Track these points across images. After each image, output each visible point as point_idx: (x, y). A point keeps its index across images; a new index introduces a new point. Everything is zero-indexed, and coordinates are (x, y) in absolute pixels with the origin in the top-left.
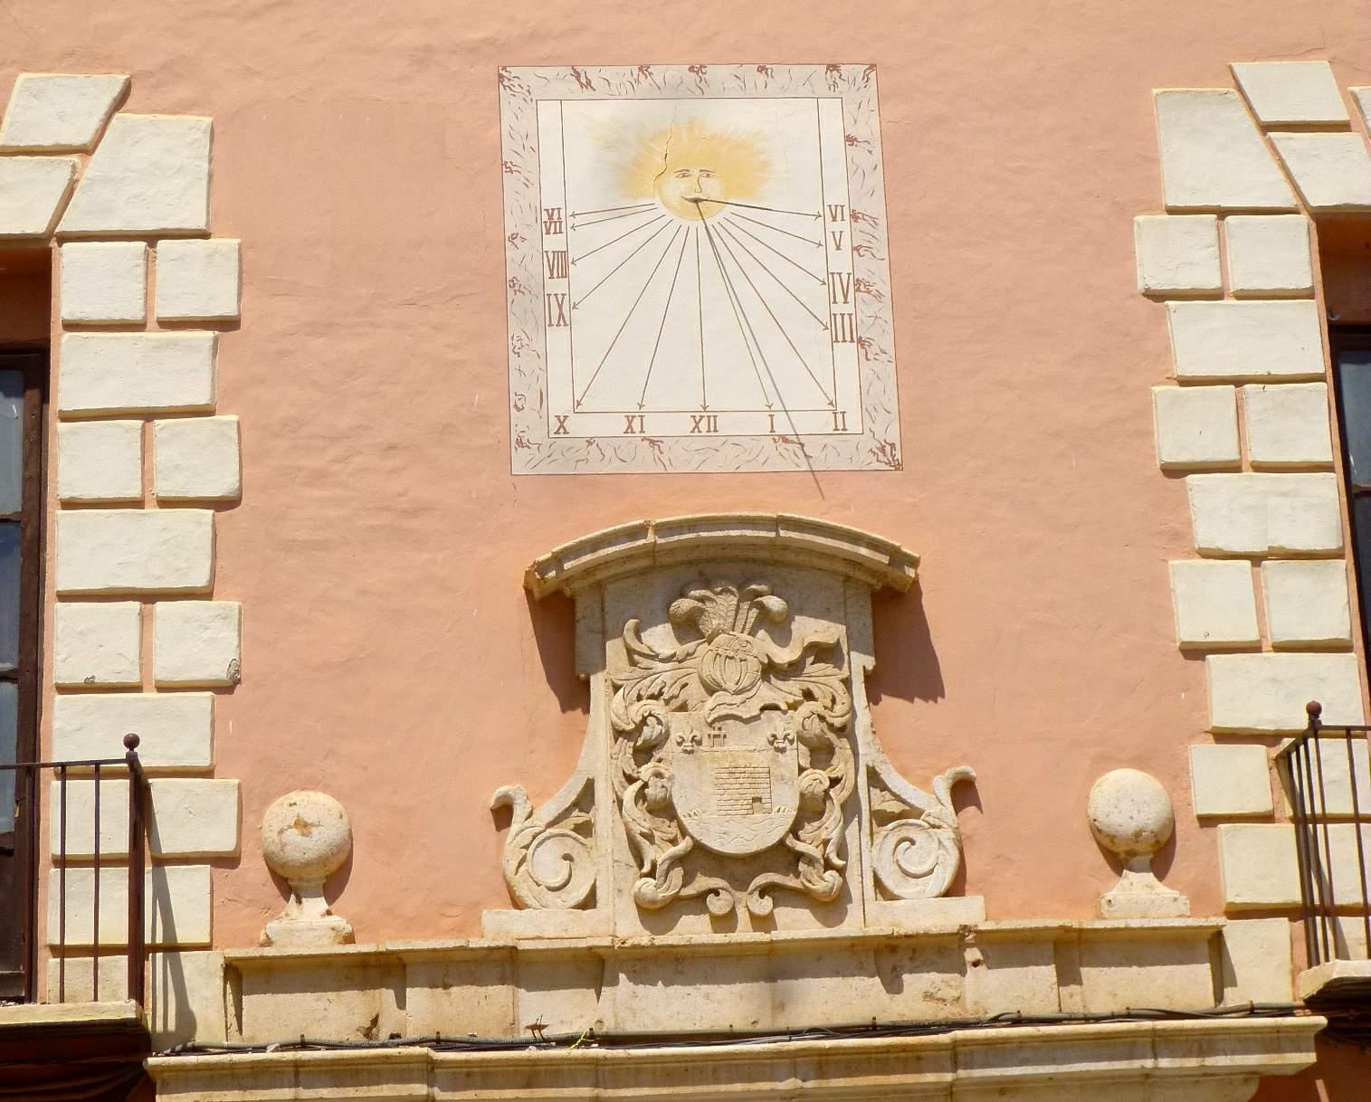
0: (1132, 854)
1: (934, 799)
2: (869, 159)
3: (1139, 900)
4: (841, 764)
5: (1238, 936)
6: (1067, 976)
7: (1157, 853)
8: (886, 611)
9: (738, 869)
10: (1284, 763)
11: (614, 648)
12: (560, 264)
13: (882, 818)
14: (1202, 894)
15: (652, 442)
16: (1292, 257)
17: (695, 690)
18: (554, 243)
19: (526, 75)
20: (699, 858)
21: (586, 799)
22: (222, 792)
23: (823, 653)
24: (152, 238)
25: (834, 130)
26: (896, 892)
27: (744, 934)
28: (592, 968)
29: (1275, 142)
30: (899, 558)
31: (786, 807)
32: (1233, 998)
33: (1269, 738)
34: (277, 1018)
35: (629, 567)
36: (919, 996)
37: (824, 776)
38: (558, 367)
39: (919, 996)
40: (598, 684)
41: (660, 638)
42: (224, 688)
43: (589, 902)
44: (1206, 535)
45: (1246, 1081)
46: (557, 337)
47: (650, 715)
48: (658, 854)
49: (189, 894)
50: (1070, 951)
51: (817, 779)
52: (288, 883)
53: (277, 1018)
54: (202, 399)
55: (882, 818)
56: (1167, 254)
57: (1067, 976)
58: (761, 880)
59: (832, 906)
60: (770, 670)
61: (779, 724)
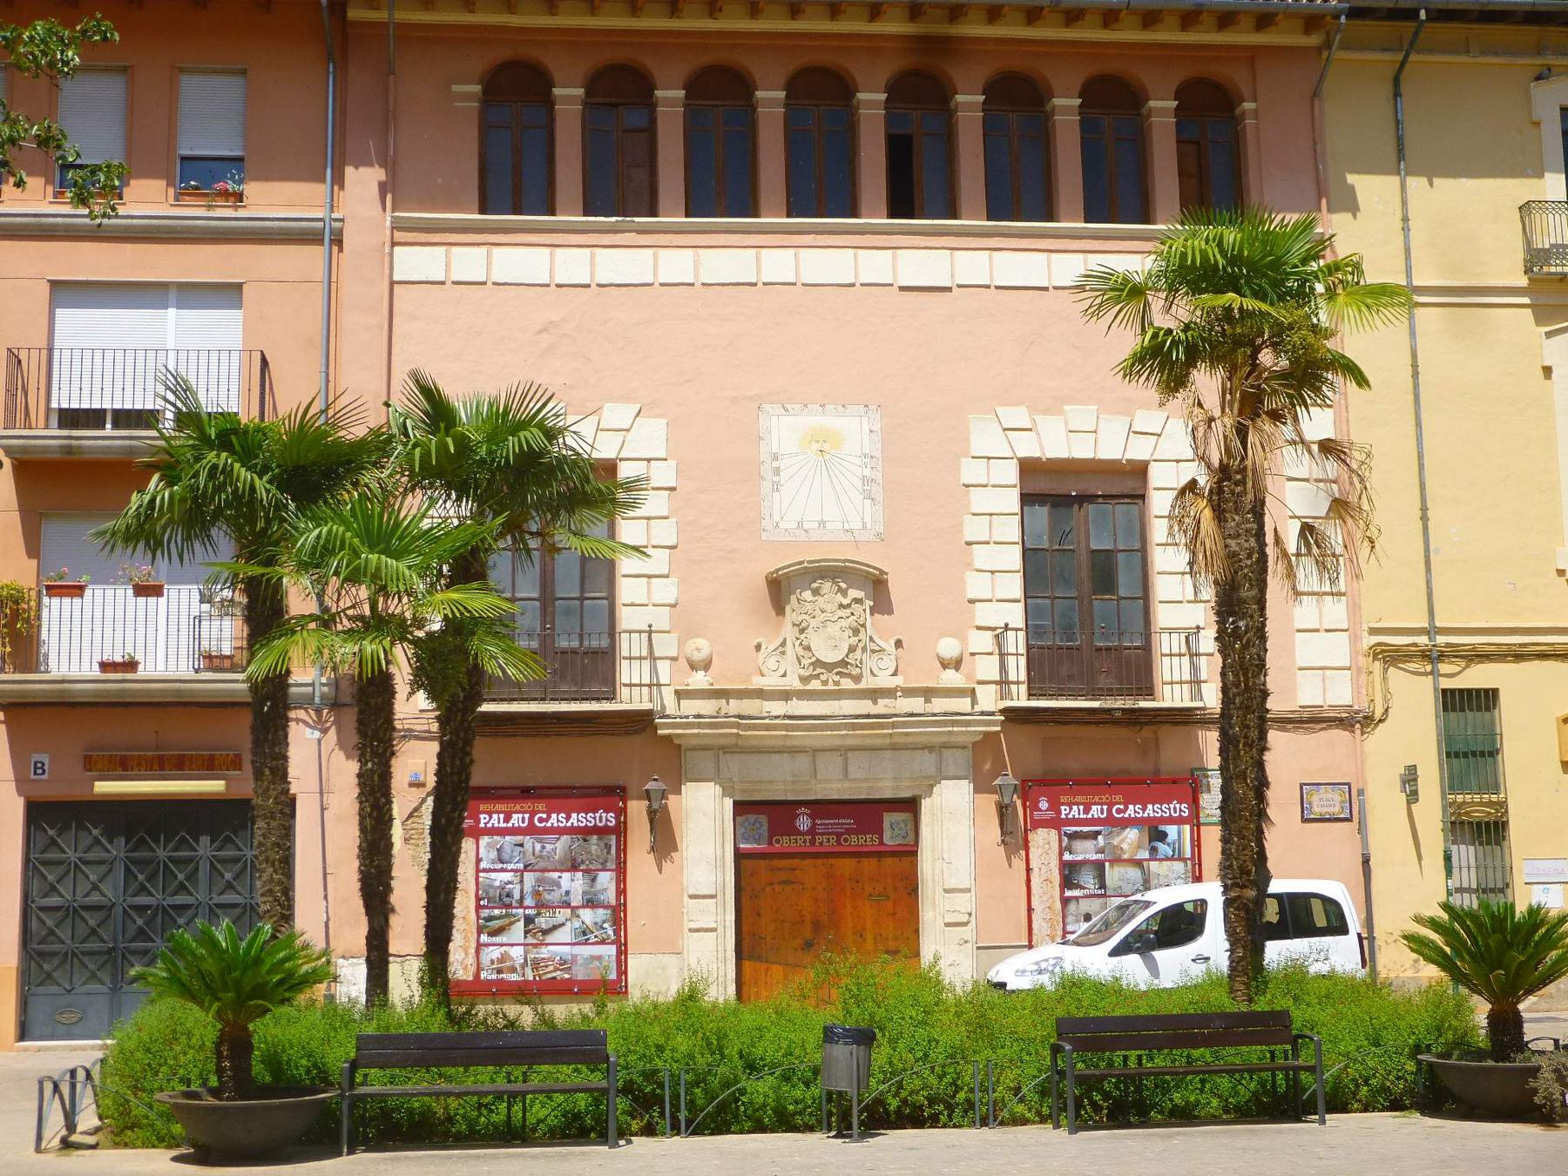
1: (889, 646)
2: (877, 437)
3: (951, 678)
4: (862, 636)
5: (979, 689)
6: (927, 701)
7: (957, 664)
8: (877, 588)
10: (997, 636)
11: (793, 598)
12: (777, 471)
13: (873, 651)
14: (969, 677)
16: (1011, 473)
17: (818, 612)
18: (775, 464)
19: (767, 407)
20: (818, 663)
21: (783, 644)
22: (673, 637)
23: (858, 601)
24: (649, 460)
25: (866, 429)
27: (831, 687)
28: (786, 695)
30: (882, 572)
32: (977, 708)
33: (994, 629)
34: (691, 707)
36: (883, 706)
38: (776, 505)
39: (883, 706)
40: (788, 609)
41: (807, 595)
42: (673, 606)
43: (784, 675)
44: (977, 565)
48: (806, 662)
49: (664, 668)
50: (928, 693)
51: (854, 640)
52: (693, 666)
53: (691, 707)
54: (665, 514)
55: (873, 651)
56: (971, 471)
57: (927, 701)
59: (857, 679)
60: (841, 606)
61: (844, 623)
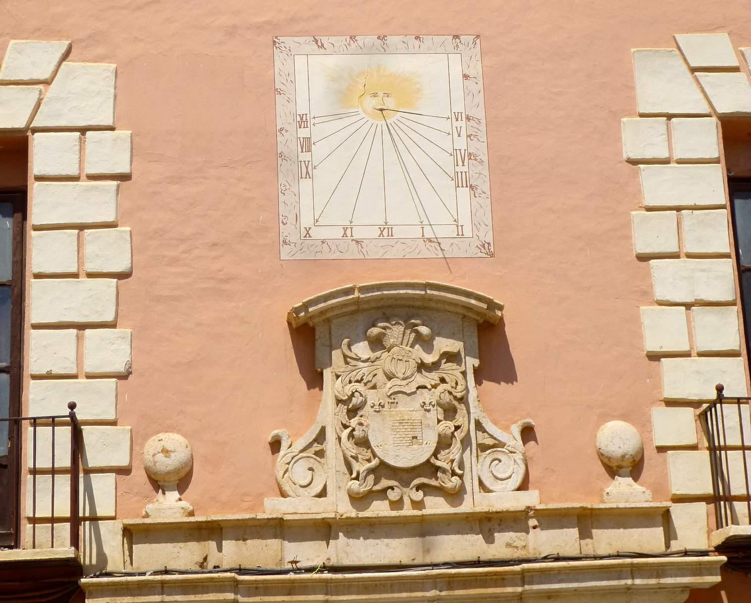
0: (620, 467)
1: (512, 437)
2: (476, 87)
3: (624, 492)
4: (461, 418)
5: (678, 512)
6: (585, 534)
7: (634, 467)
8: (485, 334)
9: (404, 475)
10: (703, 417)
11: (336, 355)
12: (307, 145)
13: (483, 448)
14: (658, 489)
15: (357, 242)
16: (708, 141)
17: (381, 377)
18: (303, 133)
19: (288, 41)
20: (383, 469)
21: (321, 437)
22: (122, 433)
23: (451, 357)
24: (83, 130)
25: (457, 71)
26: (491, 488)
27: (408, 511)
28: (325, 529)
29: (698, 77)
30: (492, 305)
31: (430, 441)
32: (675, 546)
33: (695, 404)
34: (152, 557)
35: (344, 310)
36: (504, 545)
37: (451, 424)
38: (306, 201)
39: (504, 545)
40: (328, 374)
41: (362, 349)
42: (123, 377)
43: (323, 494)
44: (661, 293)
45: (682, 591)
46: (305, 184)
47: (356, 391)
48: (360, 467)
49: (104, 489)
50: (586, 520)
51: (447, 426)
52: (158, 483)
53: (152, 557)
54: (111, 218)
55: (483, 448)
56: (639, 139)
57: (585, 534)
58: (417, 481)
59: (456, 496)
60: (422, 367)
61: (427, 396)
